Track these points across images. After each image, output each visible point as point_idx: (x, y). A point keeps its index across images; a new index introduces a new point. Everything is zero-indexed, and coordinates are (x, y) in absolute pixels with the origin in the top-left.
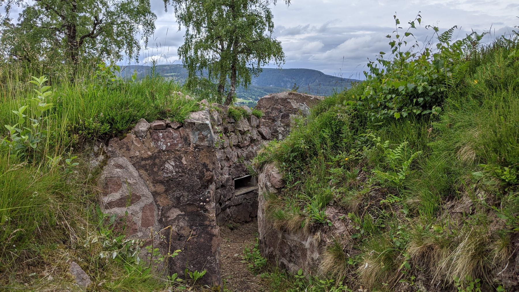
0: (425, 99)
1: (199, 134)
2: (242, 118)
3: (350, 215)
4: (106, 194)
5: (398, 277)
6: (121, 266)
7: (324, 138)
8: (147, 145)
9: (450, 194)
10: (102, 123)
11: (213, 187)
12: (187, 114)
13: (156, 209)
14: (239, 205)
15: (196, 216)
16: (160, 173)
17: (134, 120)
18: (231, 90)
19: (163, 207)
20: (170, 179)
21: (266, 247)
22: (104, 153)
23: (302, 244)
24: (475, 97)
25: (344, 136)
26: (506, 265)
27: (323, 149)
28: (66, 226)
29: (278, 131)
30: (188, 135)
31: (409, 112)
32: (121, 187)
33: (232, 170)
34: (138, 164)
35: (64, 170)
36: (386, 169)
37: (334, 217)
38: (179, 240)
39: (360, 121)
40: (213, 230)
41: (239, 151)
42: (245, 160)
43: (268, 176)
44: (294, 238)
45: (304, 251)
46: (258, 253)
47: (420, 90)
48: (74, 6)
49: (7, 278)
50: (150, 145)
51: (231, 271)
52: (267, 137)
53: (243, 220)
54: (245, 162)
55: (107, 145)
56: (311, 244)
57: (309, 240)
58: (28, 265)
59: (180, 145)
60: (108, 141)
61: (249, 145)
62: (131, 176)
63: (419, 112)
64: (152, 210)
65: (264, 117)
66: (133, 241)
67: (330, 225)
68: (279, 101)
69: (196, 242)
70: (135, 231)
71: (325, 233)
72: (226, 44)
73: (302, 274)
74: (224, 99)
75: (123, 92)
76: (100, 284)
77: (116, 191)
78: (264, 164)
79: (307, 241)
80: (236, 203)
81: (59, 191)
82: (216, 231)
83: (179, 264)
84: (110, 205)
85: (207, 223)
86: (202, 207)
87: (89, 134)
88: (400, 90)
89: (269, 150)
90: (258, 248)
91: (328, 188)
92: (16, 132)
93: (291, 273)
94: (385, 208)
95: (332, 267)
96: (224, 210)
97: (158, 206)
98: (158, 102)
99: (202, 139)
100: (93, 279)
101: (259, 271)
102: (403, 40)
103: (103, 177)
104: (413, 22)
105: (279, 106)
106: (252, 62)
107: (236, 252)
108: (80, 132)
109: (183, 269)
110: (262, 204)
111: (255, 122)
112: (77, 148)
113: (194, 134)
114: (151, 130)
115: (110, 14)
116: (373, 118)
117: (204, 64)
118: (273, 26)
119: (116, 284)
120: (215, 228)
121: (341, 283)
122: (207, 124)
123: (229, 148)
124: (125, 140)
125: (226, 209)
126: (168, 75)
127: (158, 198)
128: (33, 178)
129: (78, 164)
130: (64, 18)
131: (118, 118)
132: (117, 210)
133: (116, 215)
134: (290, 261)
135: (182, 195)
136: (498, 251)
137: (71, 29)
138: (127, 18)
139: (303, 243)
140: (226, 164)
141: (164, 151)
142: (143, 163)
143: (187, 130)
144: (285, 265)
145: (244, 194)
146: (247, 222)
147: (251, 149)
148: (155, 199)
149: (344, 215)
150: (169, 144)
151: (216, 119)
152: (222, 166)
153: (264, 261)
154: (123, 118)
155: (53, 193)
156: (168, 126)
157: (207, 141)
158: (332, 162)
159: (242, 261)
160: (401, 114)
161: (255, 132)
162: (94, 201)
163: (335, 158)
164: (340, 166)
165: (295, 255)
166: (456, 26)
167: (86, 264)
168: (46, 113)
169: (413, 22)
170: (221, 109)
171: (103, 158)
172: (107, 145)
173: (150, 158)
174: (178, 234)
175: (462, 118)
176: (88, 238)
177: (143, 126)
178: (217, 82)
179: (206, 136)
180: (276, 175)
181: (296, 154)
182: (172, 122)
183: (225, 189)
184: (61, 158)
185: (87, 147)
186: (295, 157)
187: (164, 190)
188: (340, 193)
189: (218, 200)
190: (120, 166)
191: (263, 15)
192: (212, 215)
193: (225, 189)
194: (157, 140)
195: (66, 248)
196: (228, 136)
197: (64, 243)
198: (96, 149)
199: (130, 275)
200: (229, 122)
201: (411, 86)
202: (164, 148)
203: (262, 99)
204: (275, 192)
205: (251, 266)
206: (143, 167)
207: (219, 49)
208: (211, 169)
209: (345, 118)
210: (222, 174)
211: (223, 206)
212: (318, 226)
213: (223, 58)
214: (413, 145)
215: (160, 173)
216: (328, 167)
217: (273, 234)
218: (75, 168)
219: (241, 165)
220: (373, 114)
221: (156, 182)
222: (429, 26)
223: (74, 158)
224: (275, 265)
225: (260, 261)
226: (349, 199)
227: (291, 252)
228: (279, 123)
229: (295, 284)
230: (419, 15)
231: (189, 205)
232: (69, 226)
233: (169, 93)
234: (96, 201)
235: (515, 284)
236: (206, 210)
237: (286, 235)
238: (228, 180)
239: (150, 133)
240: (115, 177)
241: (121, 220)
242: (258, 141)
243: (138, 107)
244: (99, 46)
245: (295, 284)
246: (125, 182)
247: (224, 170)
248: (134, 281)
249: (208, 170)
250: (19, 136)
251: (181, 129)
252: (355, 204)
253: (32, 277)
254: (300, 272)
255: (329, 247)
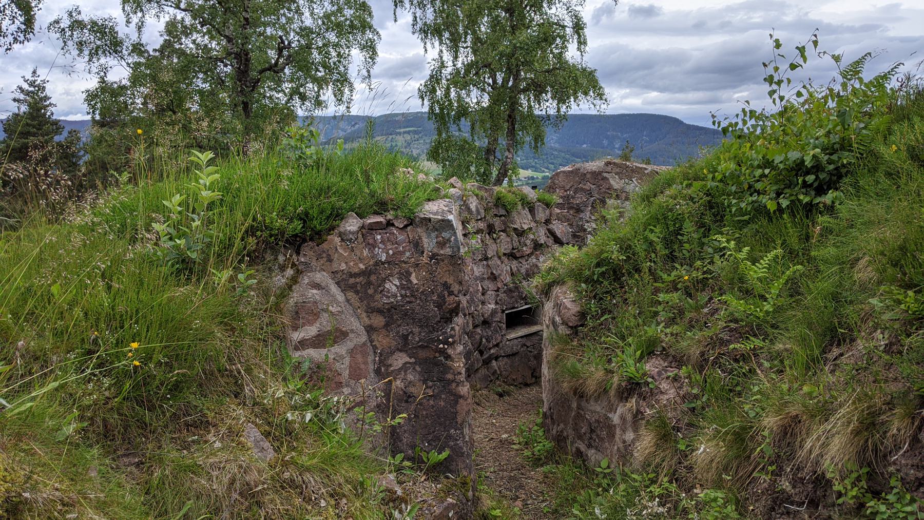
0: (817, 178)
1: (437, 237)
2: (520, 207)
3: (683, 371)
4: (295, 328)
5: (754, 470)
6: (318, 435)
7: (651, 243)
8: (358, 254)
9: (835, 336)
10: (291, 220)
11: (459, 320)
12: (417, 205)
13: (371, 353)
14: (514, 355)
15: (433, 366)
16: (378, 296)
17: (338, 215)
18: (507, 157)
19: (382, 350)
20: (393, 307)
21: (553, 423)
22: (294, 265)
23: (608, 418)
24: (889, 175)
25: (685, 238)
26: (905, 444)
27: (650, 261)
28: (239, 373)
29: (585, 230)
30: (420, 238)
31: (793, 198)
32: (318, 317)
33: (502, 296)
34: (345, 282)
35: (235, 289)
36: (747, 293)
37: (659, 373)
38: (407, 402)
39: (714, 212)
40: (460, 388)
41: (514, 264)
42: (524, 279)
43: (558, 306)
44: (596, 408)
45: (611, 428)
46: (541, 433)
47: (808, 162)
48: (246, 19)
49: (159, 441)
50: (362, 253)
51: (495, 460)
52: (564, 240)
53: (520, 380)
54: (525, 283)
55: (298, 254)
56: (623, 418)
57: (620, 410)
58: (187, 425)
59: (408, 254)
60: (299, 246)
61: (532, 254)
62: (334, 301)
63: (807, 199)
64: (365, 354)
65: (559, 206)
66: (336, 399)
67: (651, 386)
68: (588, 176)
69: (433, 407)
70: (339, 385)
71: (644, 400)
72: (500, 78)
73: (609, 467)
74: (495, 172)
75: (323, 170)
76: (287, 458)
77: (311, 323)
78: (550, 285)
79: (615, 412)
80: (509, 351)
81: (229, 321)
82: (464, 389)
83: (406, 439)
84: (302, 344)
85: (449, 376)
86: (443, 352)
87: (271, 236)
88: (776, 162)
89: (560, 262)
90: (542, 425)
91: (653, 326)
92: (169, 233)
93: (591, 465)
94: (744, 360)
95: (653, 454)
96: (487, 362)
97: (375, 347)
98: (375, 186)
99: (441, 245)
100: (277, 450)
101: (541, 462)
102: (786, 76)
103: (291, 302)
104: (804, 47)
105: (588, 186)
106: (548, 106)
107: (506, 432)
108: (259, 233)
109: (413, 447)
110: (548, 353)
111: (542, 215)
112: (254, 258)
113: (429, 236)
114: (364, 231)
115: (305, 32)
116: (734, 209)
117: (463, 111)
118: (585, 43)
119: (310, 459)
120: (463, 386)
121: (666, 479)
122: (449, 221)
123: (496, 258)
124: (325, 246)
125: (490, 361)
126: (402, 130)
127: (374, 337)
128: (192, 301)
129: (256, 281)
130: (229, 40)
131: (314, 212)
132: (312, 352)
133: (311, 361)
134: (590, 446)
135: (411, 332)
136: (897, 425)
137: (242, 58)
138: (332, 37)
139: (610, 415)
140: (491, 286)
141: (383, 263)
142: (352, 281)
143: (419, 230)
144: (581, 453)
145: (522, 337)
146: (527, 385)
147: (534, 260)
148: (369, 337)
149: (676, 371)
150: (391, 252)
151: (474, 210)
152: (483, 289)
153: (549, 445)
154: (322, 212)
155: (221, 323)
156: (390, 224)
157: (450, 247)
158: (663, 282)
159: (514, 446)
160: (778, 203)
161: (542, 231)
162: (278, 338)
163: (669, 275)
164: (677, 290)
165: (597, 435)
166: (870, 54)
167: (267, 428)
168: (211, 206)
169: (804, 47)
170: (482, 193)
171: (292, 272)
172: (298, 254)
173: (362, 273)
174: (405, 393)
175: (875, 209)
176: (270, 391)
177: (352, 224)
178: (482, 142)
179: (449, 240)
180: (569, 305)
181: (604, 269)
182: (396, 217)
183: (489, 327)
184: (231, 273)
185: (269, 257)
186: (603, 274)
187: (383, 324)
188: (672, 334)
189: (476, 346)
190: (317, 286)
191: (568, 22)
192: (459, 365)
193: (489, 327)
194: (372, 246)
195: (240, 404)
196: (494, 239)
197: (236, 397)
198: (281, 258)
199: (331, 448)
200: (496, 215)
201: (794, 155)
202: (384, 259)
203: (557, 174)
204: (568, 333)
205: (527, 453)
206: (352, 288)
207: (489, 84)
208: (456, 292)
209: (683, 207)
210: (483, 303)
211: (485, 356)
212: (633, 388)
213: (495, 101)
214: (792, 255)
215: (378, 296)
216: (657, 291)
217: (561, 402)
218: (250, 288)
219: (517, 288)
220: (734, 201)
221: (370, 311)
222: (825, 53)
223: (249, 272)
224: (567, 454)
225: (543, 445)
226: (685, 344)
227: (592, 431)
228: (586, 215)
229: (596, 482)
230: (815, 36)
231: (422, 347)
232: (243, 372)
233: (392, 169)
234: (282, 338)
235: (920, 475)
236: (448, 357)
237: (583, 404)
238: (494, 312)
239: (363, 235)
240: (309, 302)
241: (318, 367)
242: (548, 247)
243: (345, 194)
244: (287, 86)
245: (596, 482)
246: (326, 311)
247: (487, 297)
248: (336, 456)
249: (451, 293)
250: (171, 239)
251: (409, 228)
252: (695, 352)
253: (193, 441)
254: (604, 464)
255: (648, 421)
